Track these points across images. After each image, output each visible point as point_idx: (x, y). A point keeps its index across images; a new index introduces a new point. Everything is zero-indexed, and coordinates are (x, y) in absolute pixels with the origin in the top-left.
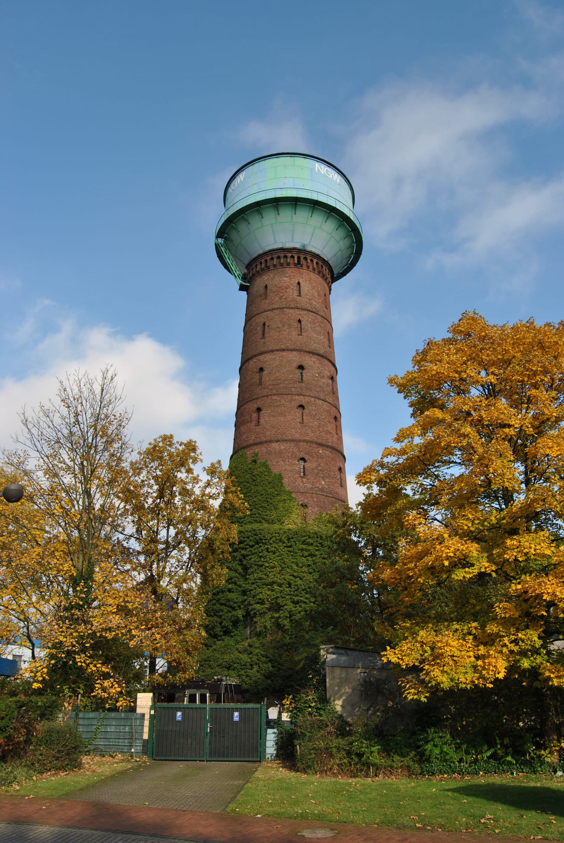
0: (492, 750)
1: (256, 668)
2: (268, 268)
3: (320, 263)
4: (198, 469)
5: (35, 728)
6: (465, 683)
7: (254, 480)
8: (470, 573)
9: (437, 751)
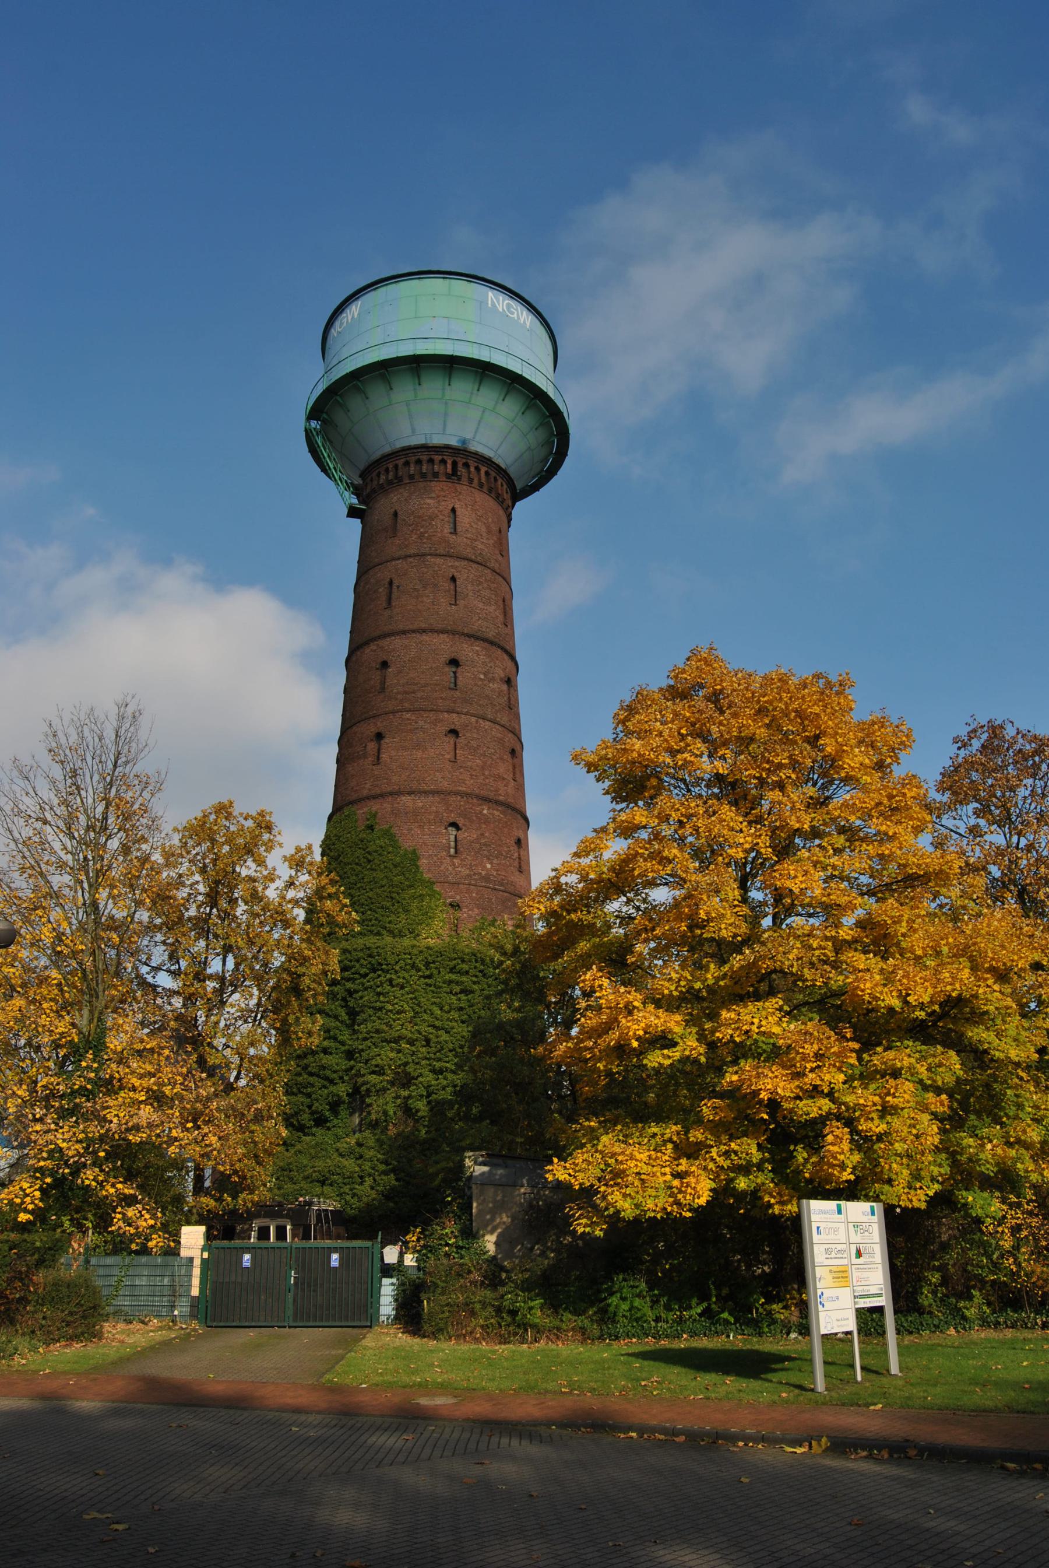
0: (705, 1305)
1: (369, 1181)
2: (399, 479)
3: (493, 474)
4: (275, 859)
5: (31, 1280)
6: (654, 1211)
7: (369, 861)
8: (669, 1057)
9: (625, 1306)
